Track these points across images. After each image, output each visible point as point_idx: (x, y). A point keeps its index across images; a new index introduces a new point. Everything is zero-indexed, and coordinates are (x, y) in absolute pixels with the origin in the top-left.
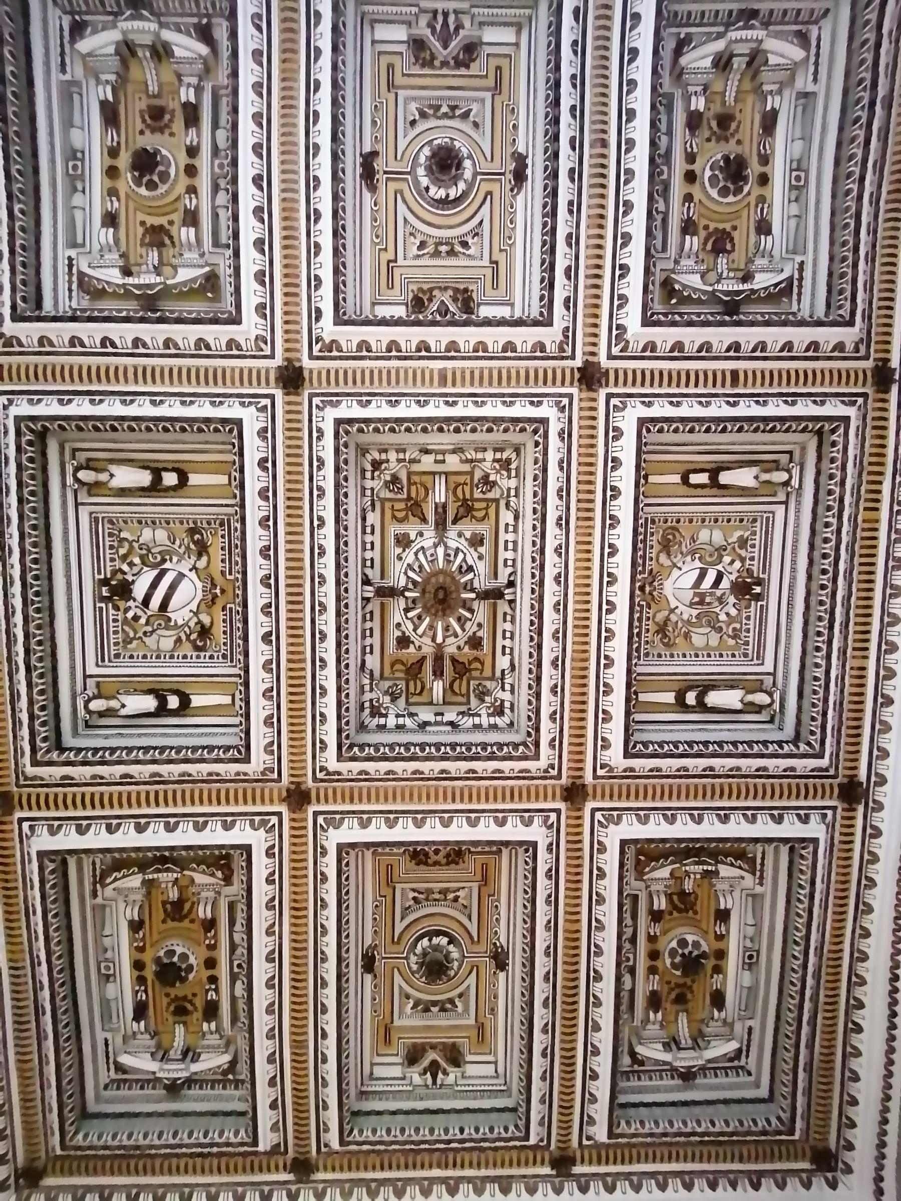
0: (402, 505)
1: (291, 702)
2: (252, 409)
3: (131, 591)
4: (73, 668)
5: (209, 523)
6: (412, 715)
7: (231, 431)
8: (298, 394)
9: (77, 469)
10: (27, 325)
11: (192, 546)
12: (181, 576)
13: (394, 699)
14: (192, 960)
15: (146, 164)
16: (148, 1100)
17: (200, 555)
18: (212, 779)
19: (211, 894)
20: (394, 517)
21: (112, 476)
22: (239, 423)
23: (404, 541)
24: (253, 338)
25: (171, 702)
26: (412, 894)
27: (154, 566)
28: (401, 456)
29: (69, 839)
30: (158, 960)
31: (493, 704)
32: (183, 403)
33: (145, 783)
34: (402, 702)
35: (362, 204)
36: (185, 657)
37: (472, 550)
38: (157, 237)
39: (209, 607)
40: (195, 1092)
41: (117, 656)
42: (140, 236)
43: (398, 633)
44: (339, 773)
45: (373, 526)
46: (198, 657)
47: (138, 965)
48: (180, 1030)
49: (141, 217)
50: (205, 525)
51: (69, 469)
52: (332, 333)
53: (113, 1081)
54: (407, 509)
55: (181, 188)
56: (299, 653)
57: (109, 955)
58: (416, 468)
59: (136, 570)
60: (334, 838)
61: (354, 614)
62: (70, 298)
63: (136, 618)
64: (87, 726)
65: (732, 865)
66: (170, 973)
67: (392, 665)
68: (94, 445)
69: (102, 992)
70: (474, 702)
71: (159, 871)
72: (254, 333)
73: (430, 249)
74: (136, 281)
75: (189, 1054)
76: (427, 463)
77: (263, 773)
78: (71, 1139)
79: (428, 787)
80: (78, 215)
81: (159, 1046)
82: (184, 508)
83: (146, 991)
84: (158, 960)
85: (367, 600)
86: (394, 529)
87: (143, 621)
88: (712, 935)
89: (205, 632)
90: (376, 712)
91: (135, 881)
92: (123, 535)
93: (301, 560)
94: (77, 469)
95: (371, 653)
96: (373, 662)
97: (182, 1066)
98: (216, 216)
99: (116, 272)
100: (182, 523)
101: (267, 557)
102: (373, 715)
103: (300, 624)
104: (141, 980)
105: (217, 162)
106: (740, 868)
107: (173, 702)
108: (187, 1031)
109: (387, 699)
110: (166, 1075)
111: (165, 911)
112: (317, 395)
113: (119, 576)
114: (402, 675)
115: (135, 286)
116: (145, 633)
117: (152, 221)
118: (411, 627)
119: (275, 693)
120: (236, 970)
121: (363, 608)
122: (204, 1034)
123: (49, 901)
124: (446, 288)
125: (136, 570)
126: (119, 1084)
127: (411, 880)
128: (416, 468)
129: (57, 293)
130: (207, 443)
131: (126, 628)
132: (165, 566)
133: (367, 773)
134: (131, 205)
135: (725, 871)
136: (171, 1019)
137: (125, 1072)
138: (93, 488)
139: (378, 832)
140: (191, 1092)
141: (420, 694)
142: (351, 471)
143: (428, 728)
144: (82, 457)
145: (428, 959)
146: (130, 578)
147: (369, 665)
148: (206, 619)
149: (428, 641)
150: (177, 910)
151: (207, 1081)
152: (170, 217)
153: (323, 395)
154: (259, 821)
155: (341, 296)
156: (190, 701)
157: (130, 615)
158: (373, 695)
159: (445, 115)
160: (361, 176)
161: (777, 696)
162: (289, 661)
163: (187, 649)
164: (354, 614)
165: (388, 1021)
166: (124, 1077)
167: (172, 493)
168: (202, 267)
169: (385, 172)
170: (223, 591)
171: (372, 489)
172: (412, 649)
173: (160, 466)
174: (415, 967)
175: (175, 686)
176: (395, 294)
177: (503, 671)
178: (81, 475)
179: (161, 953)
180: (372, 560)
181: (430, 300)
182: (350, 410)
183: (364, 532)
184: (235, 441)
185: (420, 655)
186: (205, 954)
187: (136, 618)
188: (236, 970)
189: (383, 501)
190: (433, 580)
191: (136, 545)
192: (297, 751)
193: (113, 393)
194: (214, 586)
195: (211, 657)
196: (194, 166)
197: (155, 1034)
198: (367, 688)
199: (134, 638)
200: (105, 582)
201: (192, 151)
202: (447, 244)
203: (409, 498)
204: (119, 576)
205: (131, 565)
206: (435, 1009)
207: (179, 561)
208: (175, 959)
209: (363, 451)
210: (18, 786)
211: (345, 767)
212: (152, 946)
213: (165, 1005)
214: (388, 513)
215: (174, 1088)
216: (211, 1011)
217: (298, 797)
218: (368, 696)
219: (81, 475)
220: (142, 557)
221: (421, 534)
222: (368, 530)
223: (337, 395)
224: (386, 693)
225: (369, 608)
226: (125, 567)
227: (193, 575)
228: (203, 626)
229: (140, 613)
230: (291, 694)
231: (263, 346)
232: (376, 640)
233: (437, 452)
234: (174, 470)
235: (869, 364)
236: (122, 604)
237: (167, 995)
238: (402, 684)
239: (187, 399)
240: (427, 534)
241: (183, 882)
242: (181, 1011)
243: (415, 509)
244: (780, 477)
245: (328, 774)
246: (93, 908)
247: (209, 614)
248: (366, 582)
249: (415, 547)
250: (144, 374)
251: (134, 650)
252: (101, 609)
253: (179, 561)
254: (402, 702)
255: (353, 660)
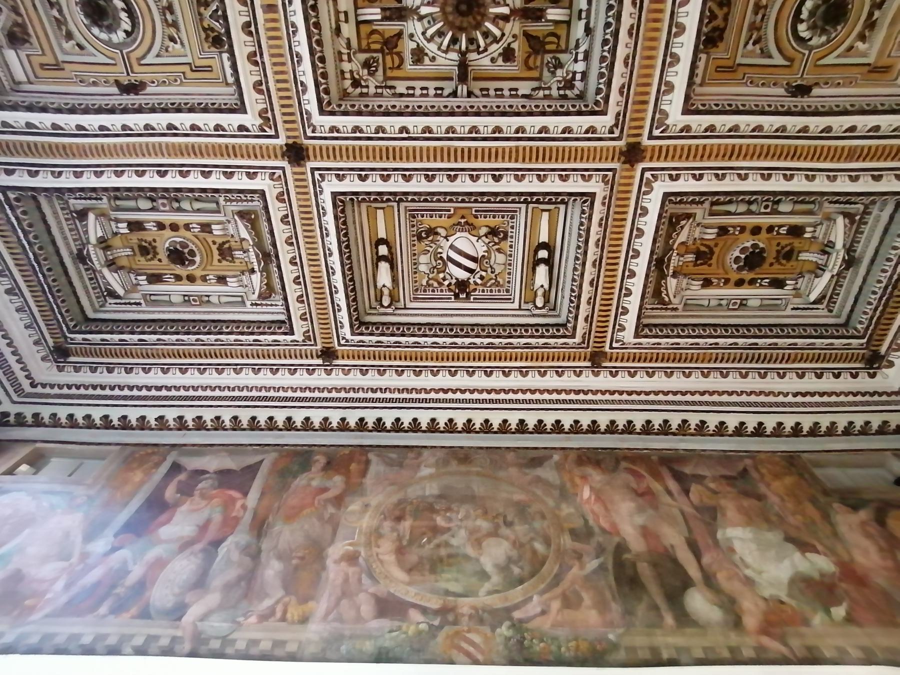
0: (388, 58)
1: (550, 159)
2: (323, 184)
3: (463, 281)
4: (513, 316)
5: (413, 226)
6: (577, 46)
7: (342, 201)
8: (307, 149)
9: (382, 306)
10: (294, 326)
11: (430, 238)
12: (452, 247)
13: (560, 65)
14: (748, 244)
15: (178, 256)
16: (852, 282)
17: (437, 234)
18: (604, 223)
19: (698, 229)
20: (399, 67)
21: (384, 286)
22: (334, 195)
23: (419, 55)
24: (272, 183)
25: (544, 254)
26: (750, 46)
27: (445, 265)
28: (345, 57)
29: (630, 321)
30: (740, 269)
31: (361, 78)
32: (327, 235)
33: (599, 271)
34: (563, 57)
35: (153, 93)
36: (511, 247)
37: (501, 50)
38: (225, 252)
39: (475, 228)
40: (859, 248)
41: (508, 291)
42: (228, 263)
43: (500, 61)
44: (618, 114)
45: (408, 88)
46: (512, 237)
47: (739, 283)
48: (804, 256)
49: (215, 262)
50: (415, 229)
51: (382, 310)
52: (253, 116)
53: (828, 306)
54: (391, 53)
55: (188, 234)
56: (510, 152)
57: (724, 302)
58: (354, 43)
59: (448, 277)
60: (676, 118)
61: (479, 102)
62: (276, 305)
63: (482, 278)
64: (554, 309)
65: (261, 282)
66: (754, 259)
67: (530, 69)
68: (366, 297)
69: (754, 309)
70: (363, 57)
71: (668, 267)
72: (268, 181)
73: (172, 31)
74: (256, 264)
75: (826, 248)
76: (348, 30)
77: (606, 183)
78: (859, 332)
79: (648, 21)
80: (224, 300)
81: (810, 272)
82: (403, 240)
83: (762, 279)
84: (740, 269)
85: (470, 94)
86: (409, 67)
87: (484, 274)
88: (204, 273)
89: (493, 232)
90: (569, 84)
91: (672, 283)
92: (424, 283)
93: (435, 149)
94: (382, 306)
95: (516, 90)
96: (525, 88)
97: (834, 255)
98: (199, 211)
99: (253, 277)
100: (414, 245)
101: (433, 177)
102: (572, 87)
103: (487, 151)
104: (752, 282)
105: (162, 208)
106: (261, 288)
107: (543, 254)
108: (807, 251)
109: (559, 72)
110: (837, 268)
111: (701, 264)
112: (305, 132)
113: (453, 287)
114: (539, 57)
115: (259, 264)
116: (492, 272)
117: (216, 256)
118: (494, 47)
119: (542, 173)
120: (768, 210)
121: (477, 97)
122: (814, 238)
123: (671, 334)
124: (200, 14)
125: (448, 277)
126: (832, 301)
127: (738, 47)
128: (354, 43)
129: (273, 312)
130: (354, 222)
131: (489, 284)
132: (445, 258)
133: (623, 86)
134: (209, 267)
135: (256, 278)
136: (792, 263)
137: (824, 297)
138: (394, 299)
139: (679, 76)
140: (859, 250)
141: (558, 37)
142: (360, 104)
143: (592, 25)
144: (374, 304)
145: (820, 23)
146: (454, 281)
147: (527, 92)
148: (484, 231)
149: (508, 27)
150: (703, 255)
151: (855, 236)
152: (211, 244)
153: (304, 127)
154: (646, 186)
155: (223, 107)
156: (544, 243)
157: (479, 281)
158: (554, 87)
159: (60, 11)
160: (137, 94)
161: (390, 310)
162: (516, 161)
163: (505, 245)
164: (479, 102)
165: (867, 68)
166: (827, 299)
167: (393, 250)
168: (235, 221)
169: (128, 74)
170: (463, 217)
171: (376, 87)
172: (515, 46)
173: (375, 257)
174: (824, 38)
175: (532, 253)
176: (215, 63)
177: (578, 40)
178: (386, 304)
179: (735, 266)
180: (436, 89)
181: (212, 30)
182: (312, 106)
183: (413, 95)
184: (348, 198)
185: (521, 38)
186: (747, 234)
187: (482, 278)
188: (768, 210)
189: (386, 78)
190: (451, 18)
191: (431, 276)
192: (591, 155)
193: (329, 280)
194: (459, 224)
195: (512, 227)
196: (170, 225)
197: (801, 275)
198: (547, 92)
199: (496, 280)
200: (457, 296)
201: (161, 226)
202: (165, 15)
203: (381, 51)
204: (453, 287)
205: (444, 279)
206: (877, 14)
207: (441, 247)
208: (743, 256)
209: (345, 95)
210: (588, 348)
211: (613, 109)
212: (727, 273)
213: (779, 267)
214: (396, 73)
215: (850, 262)
216: (796, 231)
217: (633, 154)
218: (555, 93)
219: (386, 304)
220: (439, 273)
221: (411, 36)
222: (411, 92)
223: (301, 114)
224: (553, 74)
225: (477, 92)
226: (446, 283)
227: (451, 239)
228: (489, 233)
229: (478, 275)
230: (544, 159)
231: (276, 176)
232: (506, 85)
233: (338, 21)
234: (377, 248)
235: (607, 349)
236: (472, 287)
237: (771, 264)
238: (548, 57)
239: (324, 234)
240: (411, 30)
241: (683, 250)
242: (789, 255)
243: (391, 44)
244: (540, 302)
245: (616, 125)
246: (684, 310)
247: (480, 228)
248: (454, 94)
249: (423, 43)
250: (313, 260)
251: (504, 280)
252: (474, 299)
253: (441, 247)
254: (563, 57)
255: (518, 103)
